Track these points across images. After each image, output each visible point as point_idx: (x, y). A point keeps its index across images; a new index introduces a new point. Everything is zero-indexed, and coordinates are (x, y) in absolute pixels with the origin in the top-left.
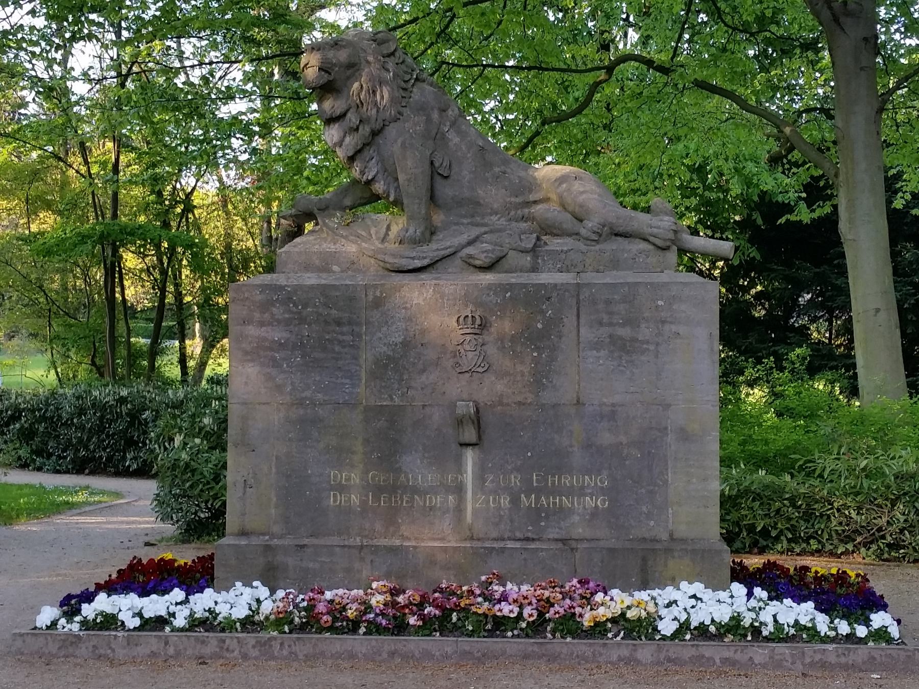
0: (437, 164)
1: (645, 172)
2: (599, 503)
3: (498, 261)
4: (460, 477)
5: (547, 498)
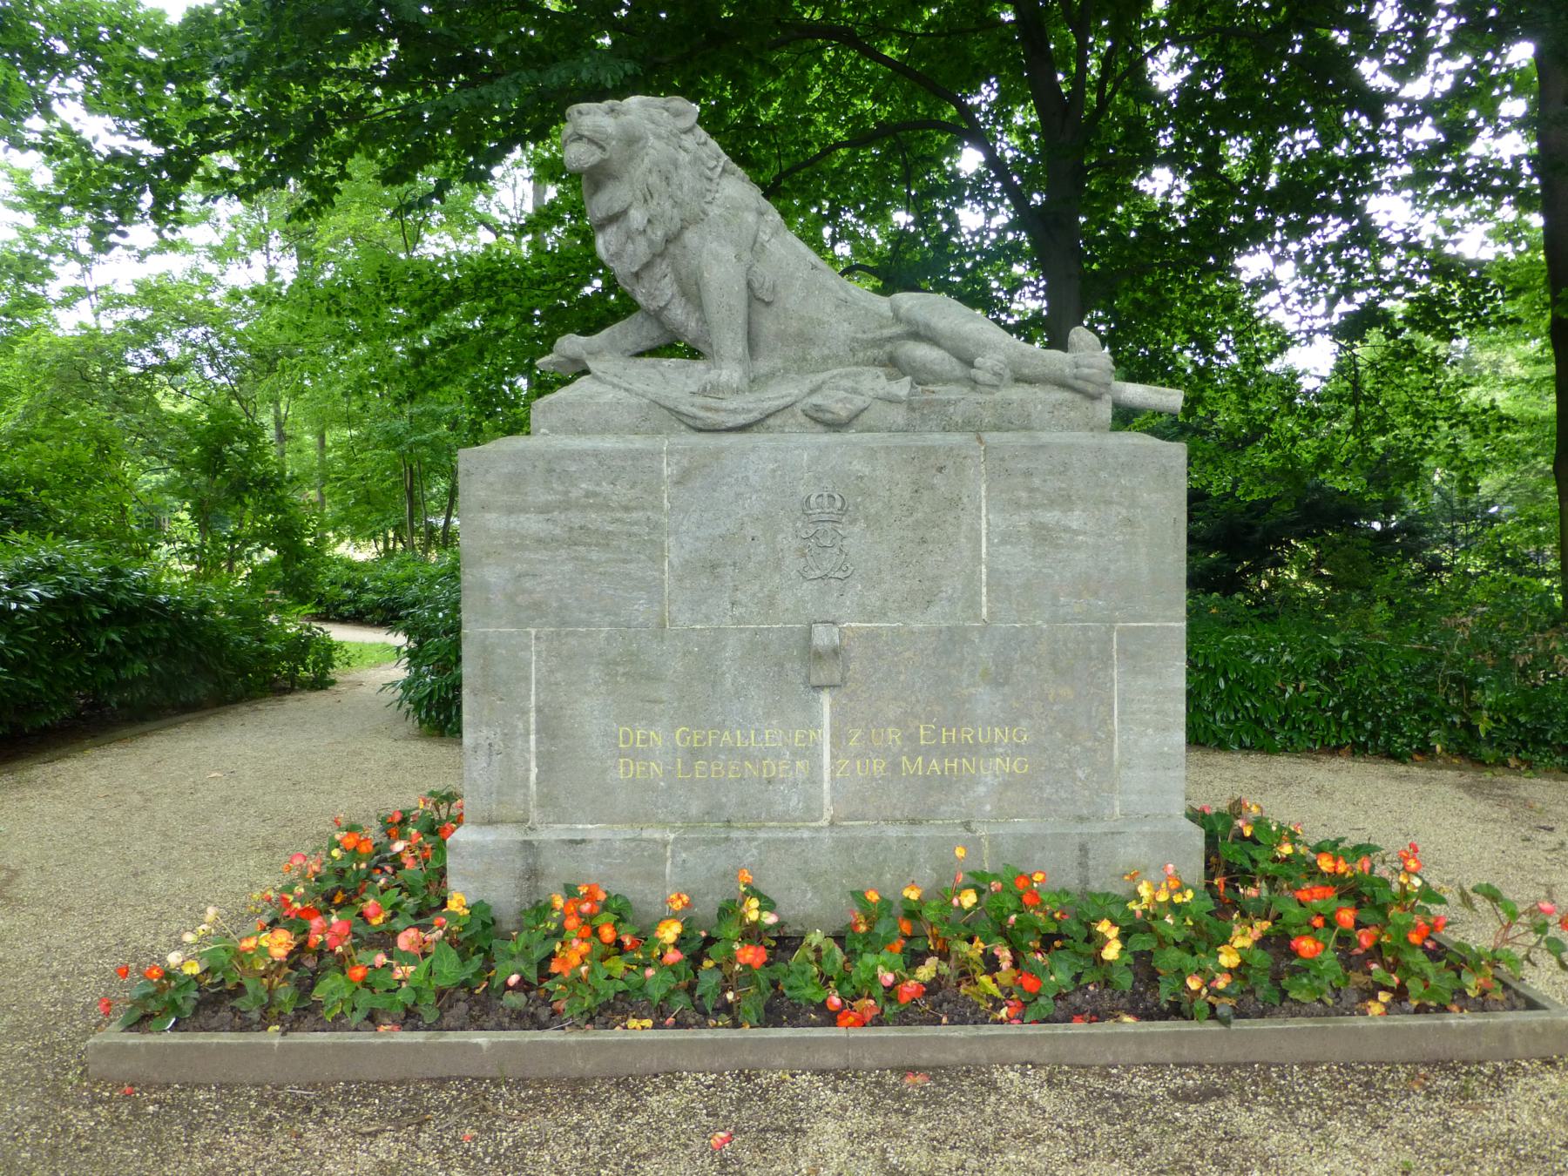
0: (756, 285)
1: (671, 167)
2: (1015, 767)
3: (857, 416)
4: (812, 733)
5: (941, 762)
